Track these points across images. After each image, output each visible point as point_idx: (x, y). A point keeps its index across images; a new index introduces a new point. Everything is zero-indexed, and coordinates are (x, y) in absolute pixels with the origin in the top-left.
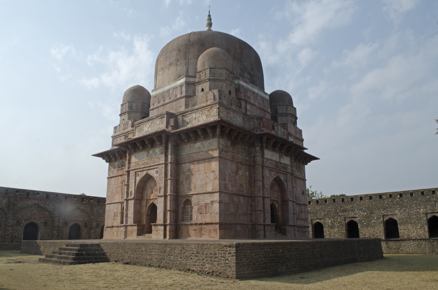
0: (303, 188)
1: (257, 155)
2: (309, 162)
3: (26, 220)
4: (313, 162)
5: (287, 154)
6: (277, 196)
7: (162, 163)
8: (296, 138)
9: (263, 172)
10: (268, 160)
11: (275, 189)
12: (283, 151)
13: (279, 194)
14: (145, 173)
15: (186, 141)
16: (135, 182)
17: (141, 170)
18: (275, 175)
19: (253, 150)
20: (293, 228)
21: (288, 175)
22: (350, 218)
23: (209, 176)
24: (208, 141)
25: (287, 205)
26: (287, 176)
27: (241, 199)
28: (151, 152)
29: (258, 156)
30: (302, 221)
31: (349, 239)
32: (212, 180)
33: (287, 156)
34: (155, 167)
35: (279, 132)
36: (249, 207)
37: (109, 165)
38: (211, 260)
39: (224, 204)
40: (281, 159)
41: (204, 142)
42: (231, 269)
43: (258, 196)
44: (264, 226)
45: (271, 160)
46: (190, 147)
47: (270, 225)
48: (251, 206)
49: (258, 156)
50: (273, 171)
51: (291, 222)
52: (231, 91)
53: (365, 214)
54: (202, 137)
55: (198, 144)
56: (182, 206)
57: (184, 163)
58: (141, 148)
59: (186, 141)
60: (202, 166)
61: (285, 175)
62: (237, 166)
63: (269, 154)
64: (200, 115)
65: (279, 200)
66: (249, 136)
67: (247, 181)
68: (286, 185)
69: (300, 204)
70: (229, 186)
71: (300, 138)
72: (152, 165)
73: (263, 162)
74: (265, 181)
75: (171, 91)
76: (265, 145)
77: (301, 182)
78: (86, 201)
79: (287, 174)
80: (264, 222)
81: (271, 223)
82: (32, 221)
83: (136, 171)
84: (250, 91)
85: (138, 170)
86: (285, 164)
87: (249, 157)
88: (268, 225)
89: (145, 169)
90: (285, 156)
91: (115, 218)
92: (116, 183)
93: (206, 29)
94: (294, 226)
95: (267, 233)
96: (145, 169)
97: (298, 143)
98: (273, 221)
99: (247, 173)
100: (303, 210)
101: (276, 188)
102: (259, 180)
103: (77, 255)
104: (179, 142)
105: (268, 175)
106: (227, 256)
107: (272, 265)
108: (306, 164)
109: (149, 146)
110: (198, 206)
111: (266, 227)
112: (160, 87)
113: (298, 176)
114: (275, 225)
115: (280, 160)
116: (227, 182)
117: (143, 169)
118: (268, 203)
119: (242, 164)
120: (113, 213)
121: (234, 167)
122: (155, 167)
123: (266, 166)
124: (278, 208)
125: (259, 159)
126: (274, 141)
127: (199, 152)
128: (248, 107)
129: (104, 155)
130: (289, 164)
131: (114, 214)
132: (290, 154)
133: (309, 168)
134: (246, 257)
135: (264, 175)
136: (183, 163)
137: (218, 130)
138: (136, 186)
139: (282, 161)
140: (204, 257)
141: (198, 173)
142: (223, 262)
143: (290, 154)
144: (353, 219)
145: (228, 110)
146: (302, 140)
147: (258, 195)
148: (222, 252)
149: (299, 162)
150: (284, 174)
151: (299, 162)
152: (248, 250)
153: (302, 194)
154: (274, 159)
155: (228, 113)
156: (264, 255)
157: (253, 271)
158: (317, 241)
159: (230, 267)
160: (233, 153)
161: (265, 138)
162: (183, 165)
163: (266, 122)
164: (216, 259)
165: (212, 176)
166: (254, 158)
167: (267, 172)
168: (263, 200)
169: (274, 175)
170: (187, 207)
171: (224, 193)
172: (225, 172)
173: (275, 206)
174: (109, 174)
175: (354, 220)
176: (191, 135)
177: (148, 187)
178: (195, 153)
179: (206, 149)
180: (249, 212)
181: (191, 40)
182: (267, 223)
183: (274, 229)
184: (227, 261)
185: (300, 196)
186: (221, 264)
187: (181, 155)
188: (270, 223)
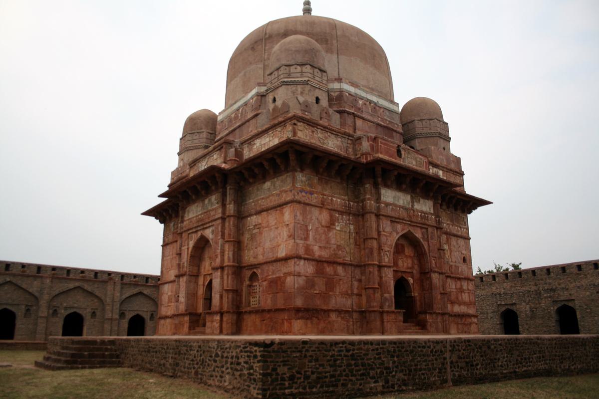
0: (464, 252)
2: (475, 208)
3: (66, 308)
5: (426, 196)
6: (410, 265)
7: (217, 217)
8: (447, 170)
9: (378, 226)
10: (387, 204)
11: (407, 254)
12: (418, 190)
13: (416, 261)
14: (199, 234)
15: (251, 180)
17: (194, 230)
20: (439, 319)
22: (561, 301)
23: (282, 234)
24: (281, 177)
25: (430, 278)
27: (340, 269)
28: (206, 201)
29: (369, 199)
34: (210, 224)
35: (410, 161)
37: (165, 227)
40: (415, 204)
41: (275, 179)
42: (257, 385)
44: (382, 313)
45: (396, 206)
46: (258, 190)
47: (393, 312)
48: (360, 281)
49: (369, 199)
50: (398, 223)
53: (588, 293)
54: (271, 172)
55: (268, 184)
56: (248, 283)
57: (251, 215)
59: (251, 180)
60: (271, 218)
61: (424, 230)
62: (331, 216)
63: (389, 195)
64: (271, 139)
65: (415, 272)
67: (352, 241)
68: (426, 247)
69: (459, 279)
71: (458, 171)
72: (207, 221)
73: (378, 208)
74: (383, 239)
76: (380, 180)
77: (461, 242)
78: (152, 283)
79: (427, 229)
80: (381, 307)
81: (396, 308)
82: (75, 310)
83: (189, 232)
86: (422, 212)
88: (388, 312)
91: (169, 304)
92: (171, 253)
95: (387, 326)
97: (453, 179)
99: (352, 227)
101: (408, 251)
102: (370, 238)
103: (73, 355)
104: (242, 183)
105: (388, 229)
106: (252, 361)
107: (351, 380)
108: (470, 212)
109: (203, 192)
110: (266, 282)
111: (385, 315)
112: (231, 105)
113: (455, 232)
115: (413, 206)
116: (311, 240)
120: (167, 296)
121: (324, 217)
122: (210, 224)
123: (383, 215)
124: (413, 284)
125: (371, 204)
126: (396, 173)
127: (269, 196)
128: (359, 123)
129: (153, 212)
130: (432, 211)
131: (169, 298)
133: (475, 218)
135: (381, 229)
136: (247, 217)
137: (292, 157)
138: (189, 255)
139: (417, 206)
140: (224, 363)
141: (267, 229)
144: (566, 303)
145: (313, 127)
146: (462, 174)
147: (369, 262)
148: (246, 354)
149: (456, 210)
150: (421, 228)
151: (456, 210)
154: (401, 203)
156: (331, 363)
157: (304, 388)
158: (460, 339)
159: (255, 380)
160: (323, 195)
161: (378, 170)
162: (249, 219)
163: (384, 144)
164: (239, 368)
165: (285, 233)
166: (363, 202)
167: (386, 226)
168: (379, 271)
169: (401, 229)
170: (254, 284)
171: (305, 259)
172: (306, 226)
173: (407, 281)
174: (164, 241)
176: (256, 170)
177: (206, 256)
178: (263, 199)
179: (278, 192)
181: (267, 32)
184: (252, 371)
185: (457, 265)
186: (244, 375)
188: (393, 308)
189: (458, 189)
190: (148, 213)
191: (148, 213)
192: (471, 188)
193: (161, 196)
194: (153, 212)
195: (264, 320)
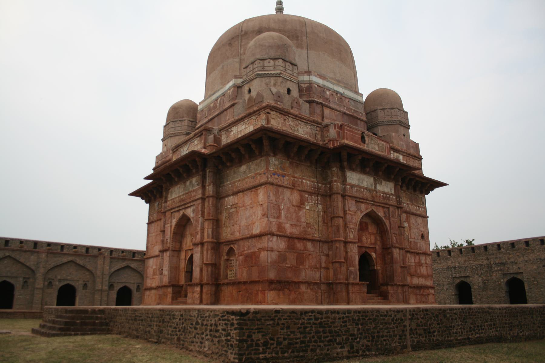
0: (422, 229)
1: (335, 179)
3: (60, 281)
4: (437, 190)
6: (373, 241)
7: (197, 197)
8: (407, 155)
10: (352, 186)
11: (370, 231)
12: (381, 173)
15: (228, 164)
16: (171, 226)
17: (176, 209)
18: (367, 209)
19: (329, 172)
21: (391, 209)
22: (511, 274)
23: (256, 213)
25: (391, 253)
26: (389, 211)
27: (309, 245)
28: (188, 183)
29: (336, 181)
30: (421, 279)
31: (461, 305)
32: (259, 217)
33: (389, 181)
35: (374, 146)
36: (324, 258)
38: (211, 335)
39: (277, 253)
40: (378, 185)
41: (251, 163)
42: (233, 350)
43: (336, 241)
44: (347, 285)
45: (360, 187)
46: (235, 173)
47: (357, 284)
49: (336, 181)
50: (362, 202)
51: (398, 280)
52: (291, 89)
53: (535, 267)
55: (243, 168)
56: (225, 257)
58: (176, 179)
59: (228, 164)
61: (386, 210)
62: (301, 197)
63: (354, 178)
65: (377, 247)
66: (319, 153)
67: (320, 219)
68: (388, 224)
69: (418, 254)
70: (287, 226)
71: (416, 155)
72: (188, 201)
73: (344, 189)
74: (349, 217)
75: (219, 100)
77: (420, 220)
78: (138, 257)
79: (389, 208)
84: (329, 89)
85: (173, 210)
87: (322, 184)
88: (353, 284)
89: (181, 208)
90: (385, 180)
93: (272, 11)
94: (403, 286)
95: (352, 296)
96: (181, 208)
98: (362, 277)
99: (320, 207)
100: (423, 261)
101: (372, 228)
102: (339, 217)
103: (66, 323)
105: (353, 208)
106: (229, 328)
107: (319, 346)
108: (428, 193)
109: (185, 175)
114: (367, 285)
115: (376, 187)
117: (179, 209)
118: (354, 252)
119: (311, 194)
121: (295, 197)
122: (192, 204)
123: (349, 196)
124: (376, 259)
125: (337, 185)
126: (360, 158)
128: (327, 111)
129: (140, 193)
130: (393, 192)
132: (393, 177)
133: (432, 199)
134: (262, 332)
135: (347, 209)
137: (266, 143)
139: (379, 188)
141: (243, 208)
142: (224, 339)
143: (393, 177)
144: (515, 276)
145: (285, 115)
147: (336, 239)
150: (383, 207)
152: (267, 320)
153: (420, 237)
154: (365, 184)
155: (285, 120)
157: (277, 353)
160: (294, 177)
162: (226, 199)
163: (350, 131)
165: (259, 212)
167: (351, 205)
168: (345, 246)
169: (364, 209)
170: (231, 258)
171: (277, 236)
172: (279, 206)
173: (370, 256)
174: (149, 219)
175: (519, 277)
177: (188, 233)
178: (239, 181)
179: (253, 174)
180: (323, 265)
182: (351, 281)
183: (365, 289)
184: (229, 338)
187: (224, 186)
188: (358, 281)
189: (416, 172)
190: (135, 194)
191: (135, 194)
192: (429, 171)
193: (147, 178)
194: (140, 193)
195: (240, 292)
